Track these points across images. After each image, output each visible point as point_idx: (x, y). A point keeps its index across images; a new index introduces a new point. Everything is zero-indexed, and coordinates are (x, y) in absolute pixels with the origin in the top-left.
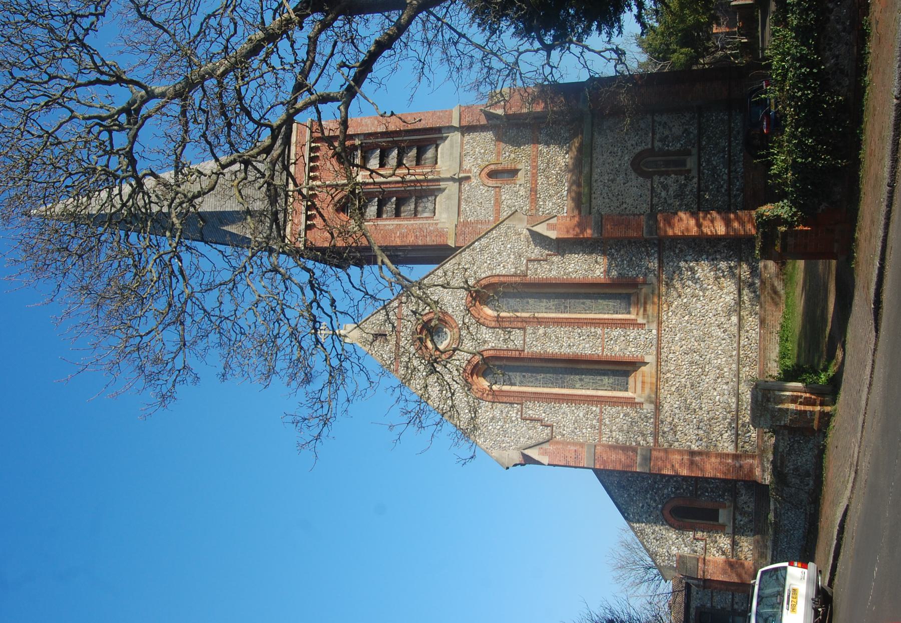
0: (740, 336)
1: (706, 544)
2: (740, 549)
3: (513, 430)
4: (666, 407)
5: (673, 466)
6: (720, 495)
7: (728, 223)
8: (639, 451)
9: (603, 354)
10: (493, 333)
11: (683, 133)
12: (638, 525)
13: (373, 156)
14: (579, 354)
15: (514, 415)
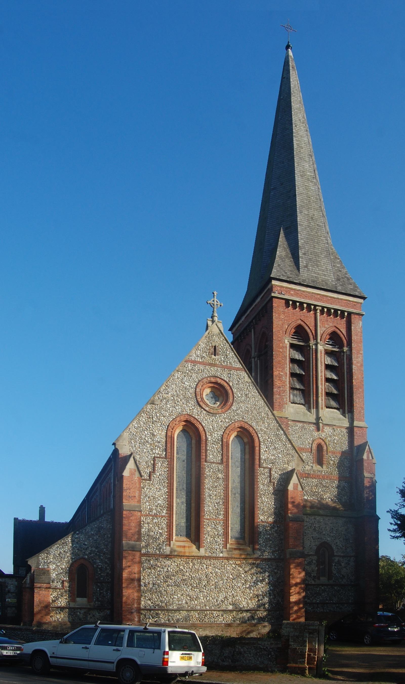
0: (219, 611)
1: (60, 589)
2: (58, 613)
3: (145, 450)
4: (168, 563)
5: (129, 566)
6: (98, 598)
7: (297, 603)
8: (138, 543)
9: (205, 519)
10: (218, 440)
11: (342, 575)
12: (70, 541)
13: (333, 360)
14: (205, 502)
15: (157, 452)
